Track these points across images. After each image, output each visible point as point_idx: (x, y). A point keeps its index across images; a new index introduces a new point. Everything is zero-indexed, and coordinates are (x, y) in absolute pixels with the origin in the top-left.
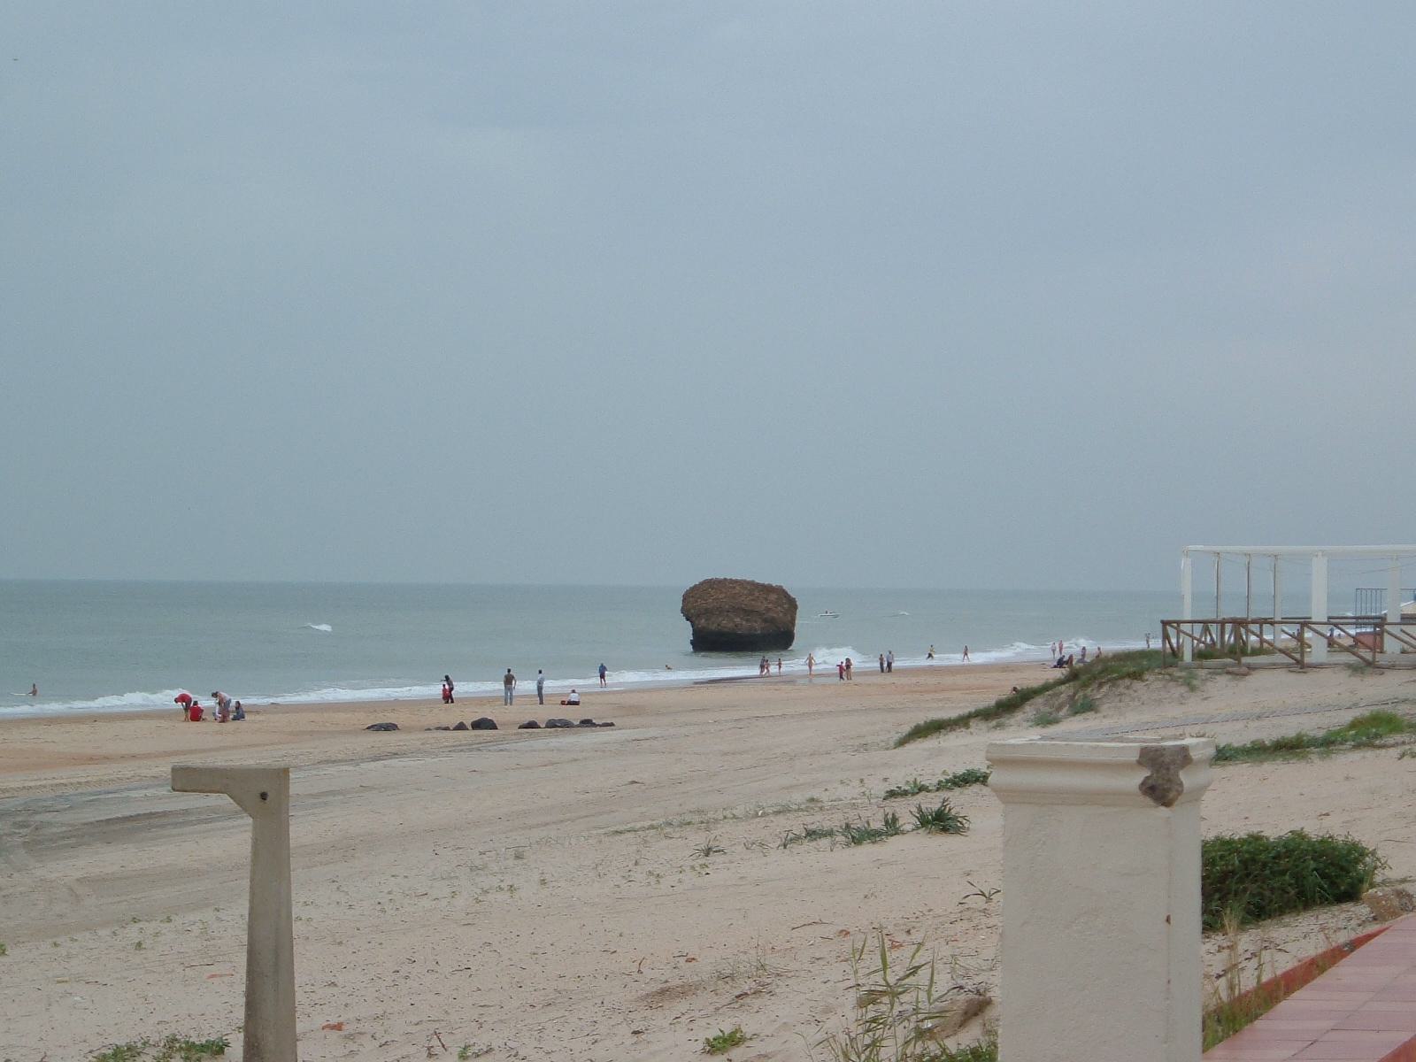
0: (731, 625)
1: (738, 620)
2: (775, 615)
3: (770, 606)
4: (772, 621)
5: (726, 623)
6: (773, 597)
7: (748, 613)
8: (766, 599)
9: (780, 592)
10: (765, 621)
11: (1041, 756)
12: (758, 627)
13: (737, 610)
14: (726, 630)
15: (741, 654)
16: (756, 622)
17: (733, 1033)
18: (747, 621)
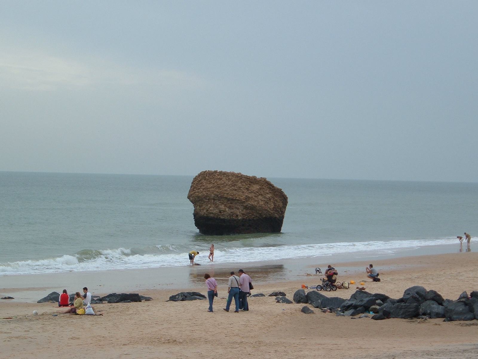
0: (216, 211)
1: (222, 207)
2: (255, 203)
3: (250, 195)
4: (252, 208)
5: (224, 211)
6: (256, 187)
7: (231, 201)
8: (247, 189)
9: (265, 184)
10: (246, 208)
11: (323, 294)
12: (239, 213)
13: (220, 198)
14: (212, 215)
15: (232, 236)
16: (238, 209)
17: (424, 313)
18: (230, 208)
